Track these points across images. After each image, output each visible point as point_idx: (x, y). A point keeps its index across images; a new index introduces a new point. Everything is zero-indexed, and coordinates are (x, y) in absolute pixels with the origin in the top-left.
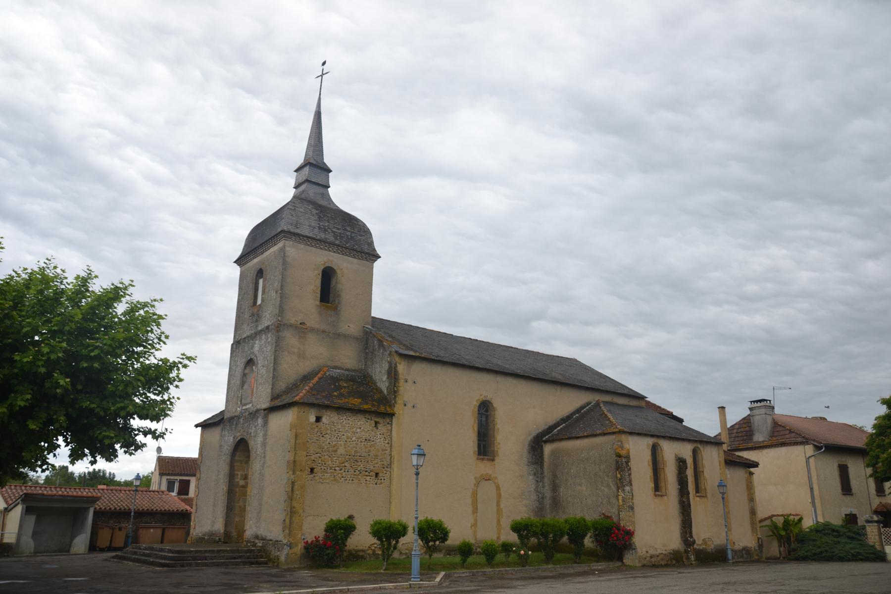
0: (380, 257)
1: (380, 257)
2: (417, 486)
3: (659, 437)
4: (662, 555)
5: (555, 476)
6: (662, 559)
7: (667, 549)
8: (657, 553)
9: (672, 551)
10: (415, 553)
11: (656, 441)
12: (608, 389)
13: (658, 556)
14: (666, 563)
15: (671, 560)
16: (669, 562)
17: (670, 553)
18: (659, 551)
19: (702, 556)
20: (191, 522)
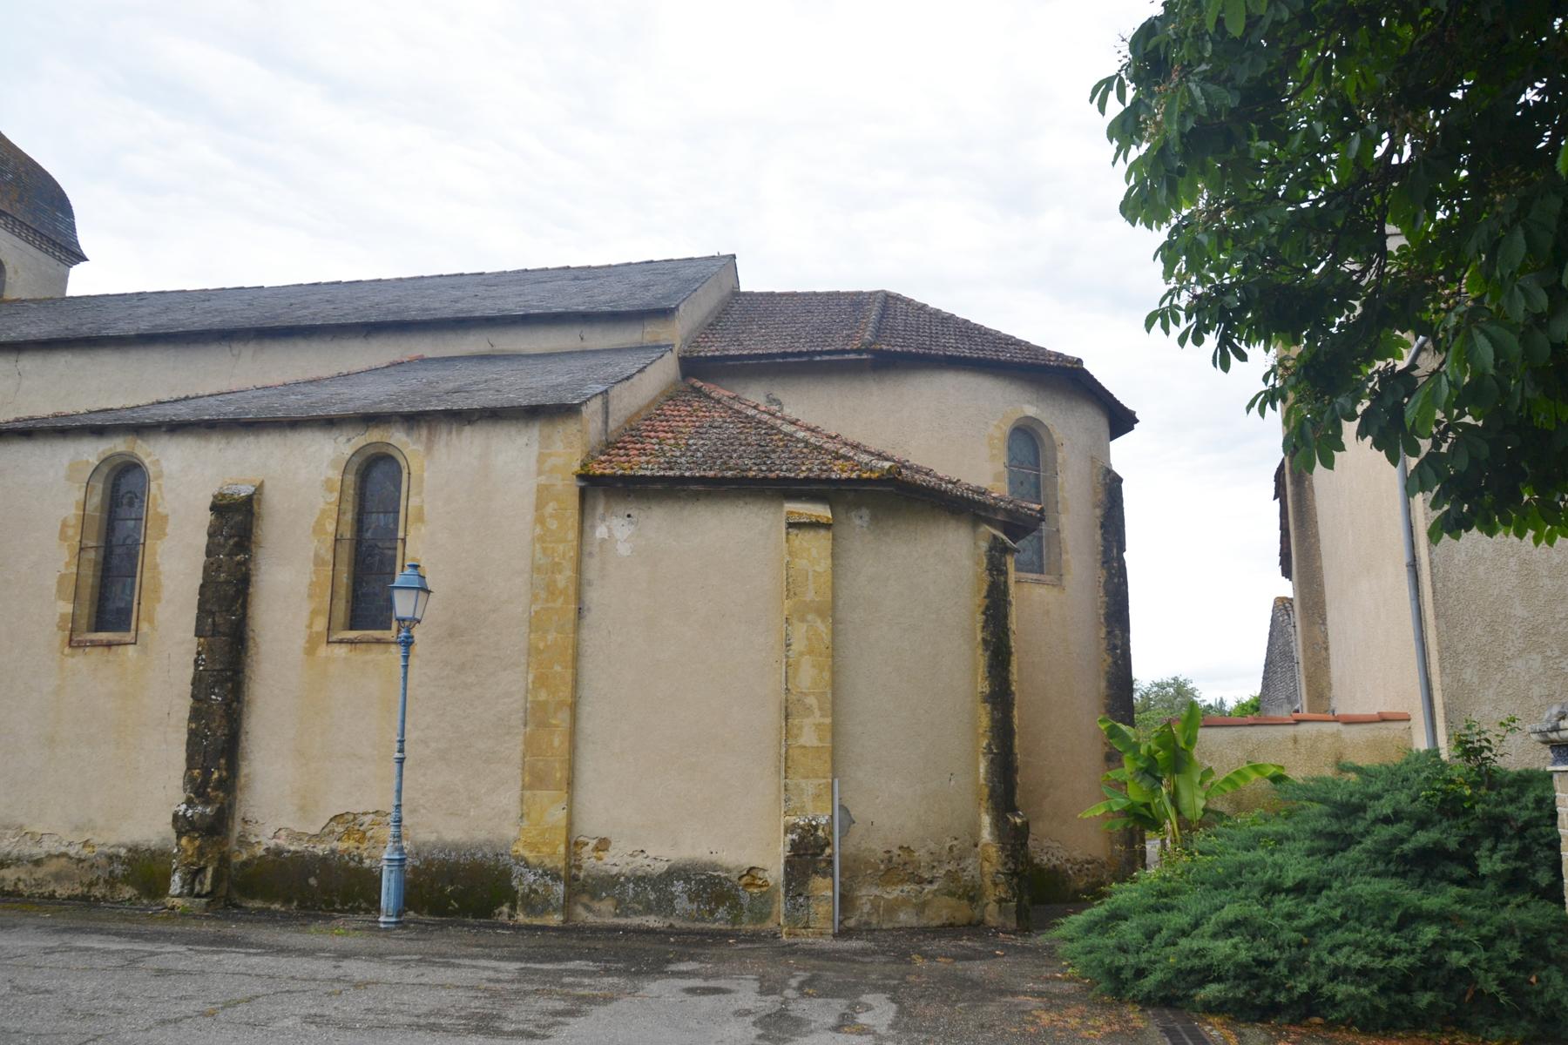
0: (85, 259)
1: (85, 259)
2: (402, 742)
3: (140, 429)
4: (63, 860)
5: (119, 644)
6: (58, 877)
7: (96, 840)
8: (38, 851)
9: (123, 852)
10: (527, 921)
11: (1030, 410)
12: (408, 316)
13: (38, 863)
14: (79, 891)
15: (112, 881)
16: (97, 892)
17: (111, 858)
18: (49, 846)
19: (312, 881)
20: (314, 856)
